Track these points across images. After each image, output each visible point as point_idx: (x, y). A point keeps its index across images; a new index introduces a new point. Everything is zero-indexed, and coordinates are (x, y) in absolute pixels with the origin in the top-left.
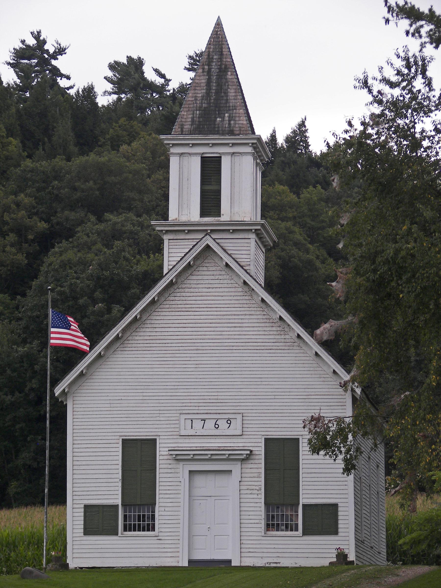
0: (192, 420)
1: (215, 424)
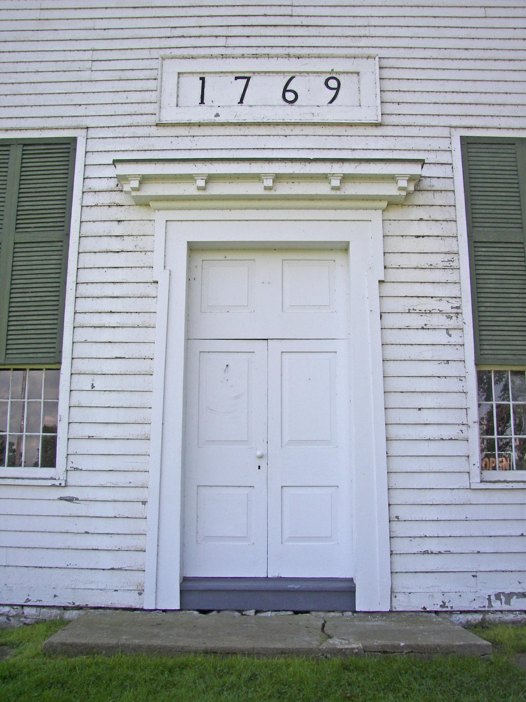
0: (203, 79)
1: (285, 90)
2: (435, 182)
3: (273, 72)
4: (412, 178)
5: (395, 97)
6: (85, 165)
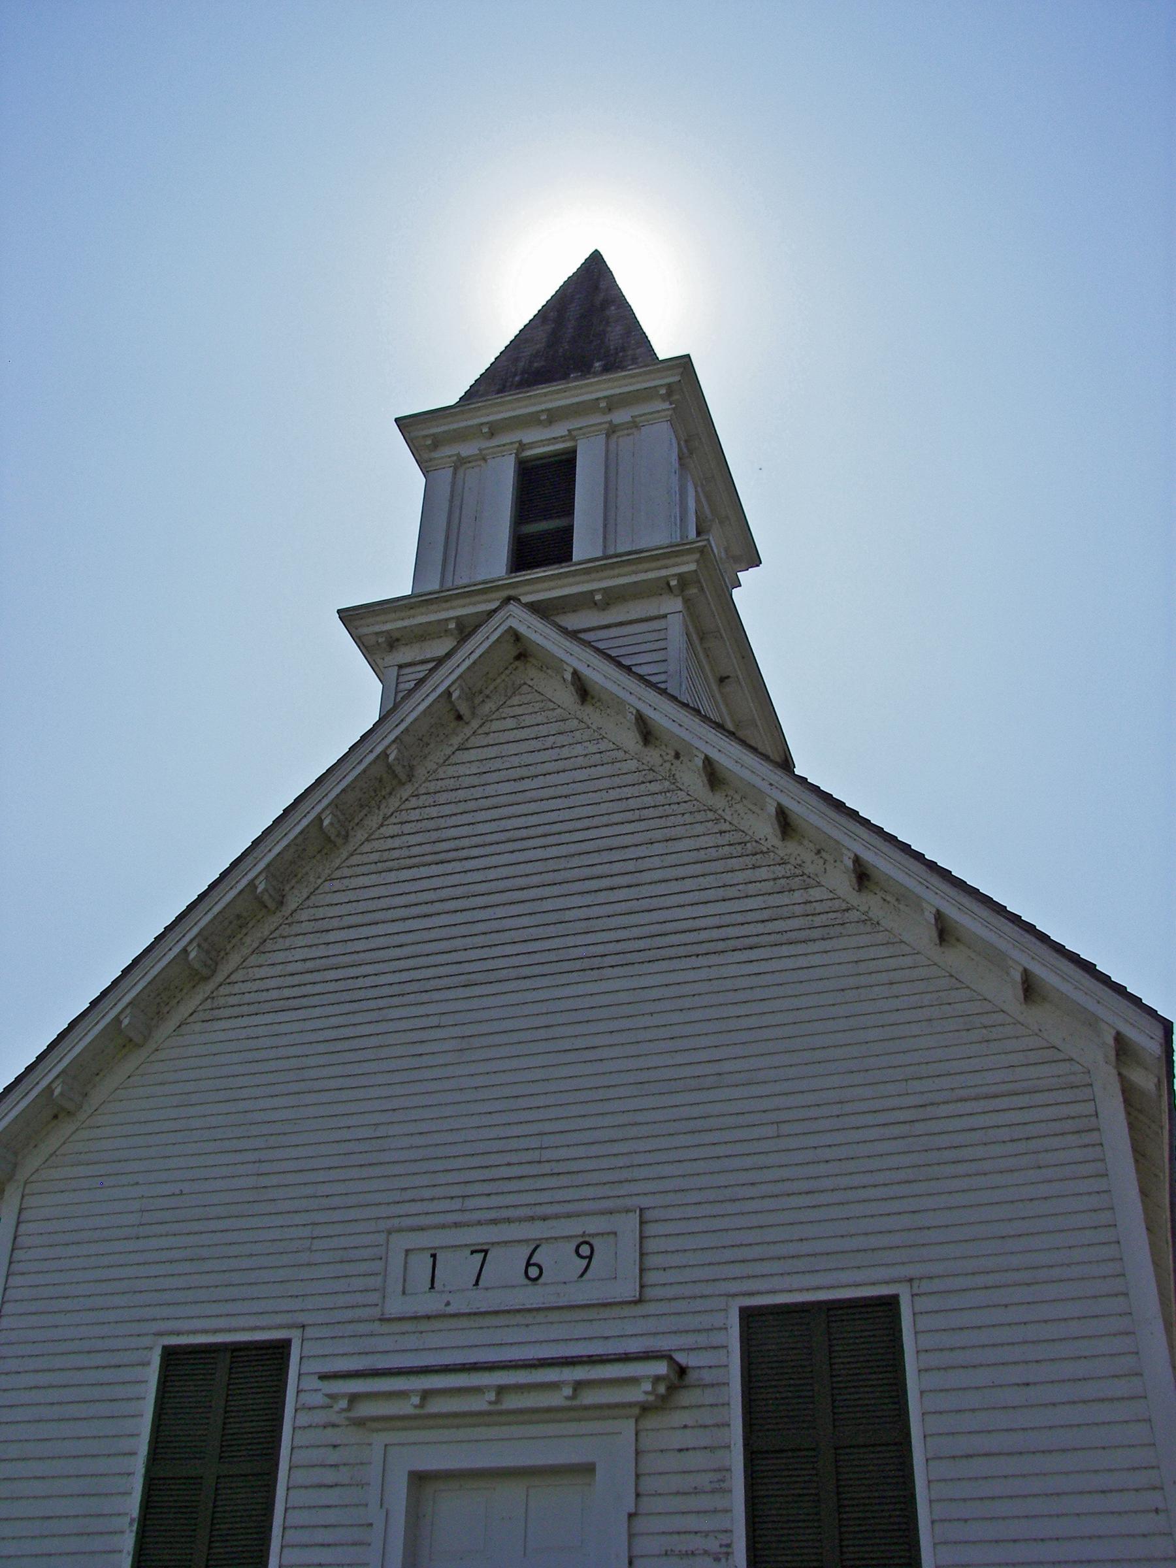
0: (434, 1256)
1: (528, 1264)
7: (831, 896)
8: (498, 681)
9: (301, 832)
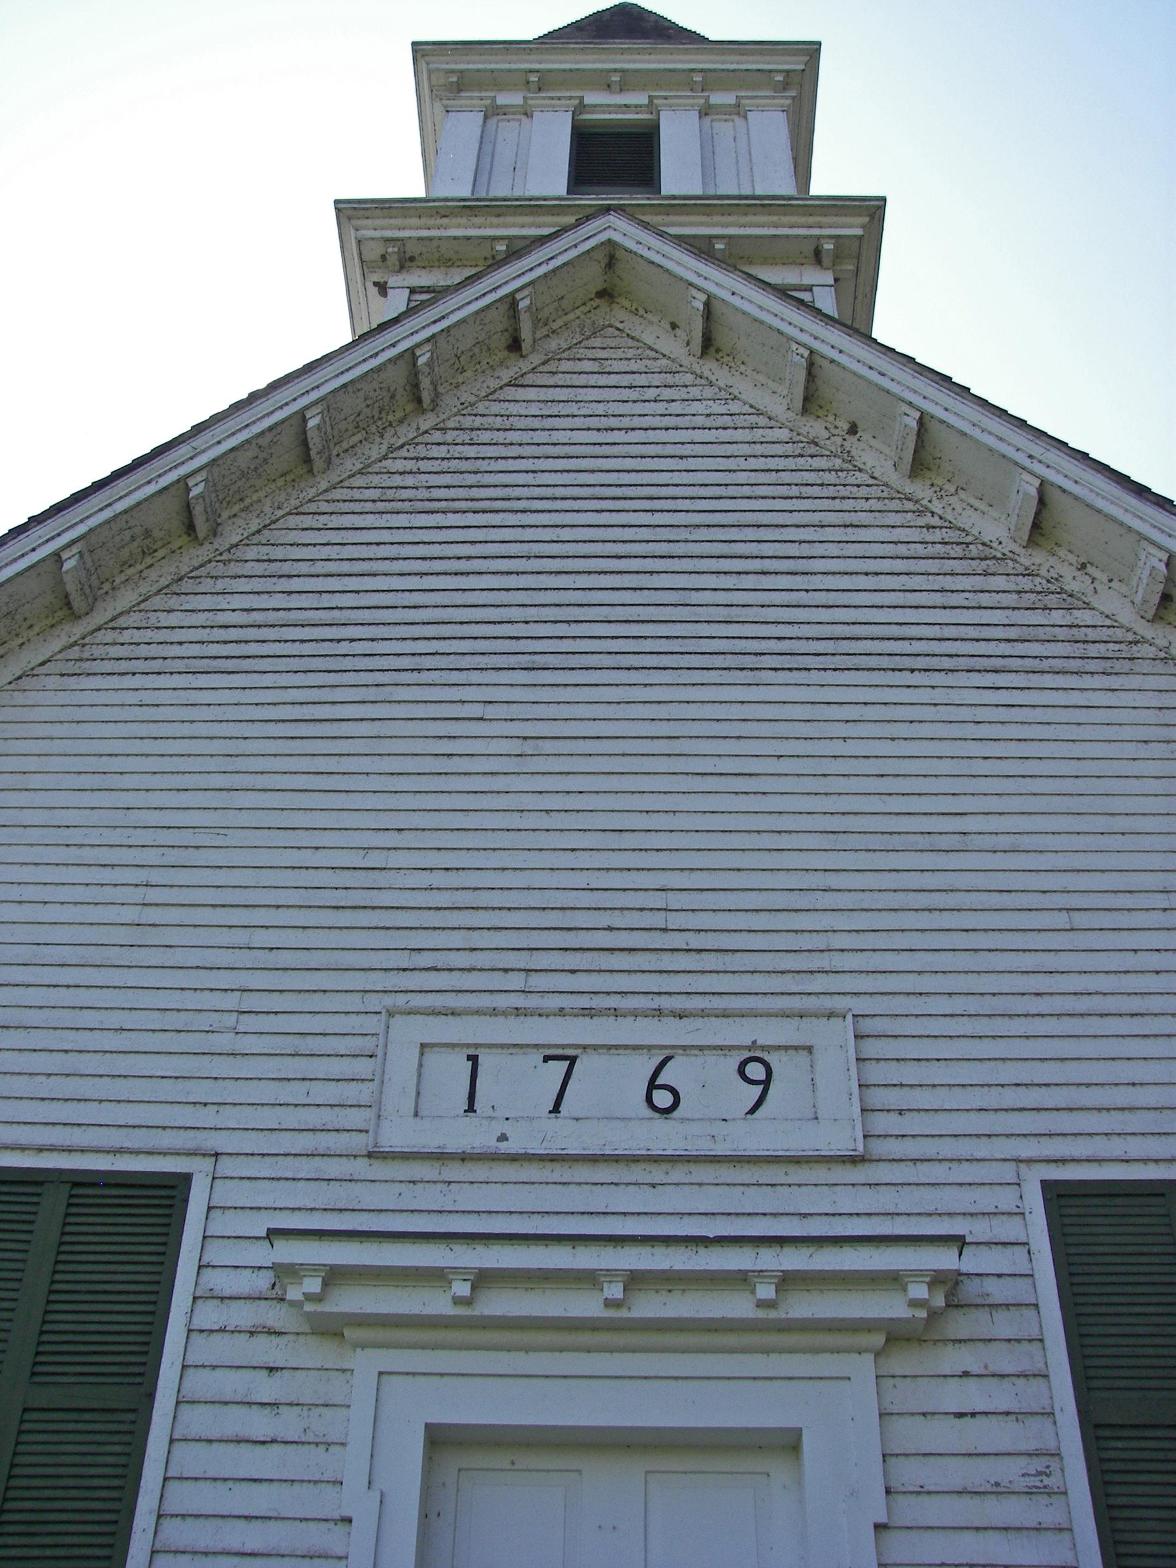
0: (474, 1059)
1: (652, 1085)
2: (991, 1286)
3: (626, 1047)
4: (938, 1279)
5: (894, 1073)
6: (204, 1237)
7: (1108, 622)
8: (571, 316)
9: (270, 429)
